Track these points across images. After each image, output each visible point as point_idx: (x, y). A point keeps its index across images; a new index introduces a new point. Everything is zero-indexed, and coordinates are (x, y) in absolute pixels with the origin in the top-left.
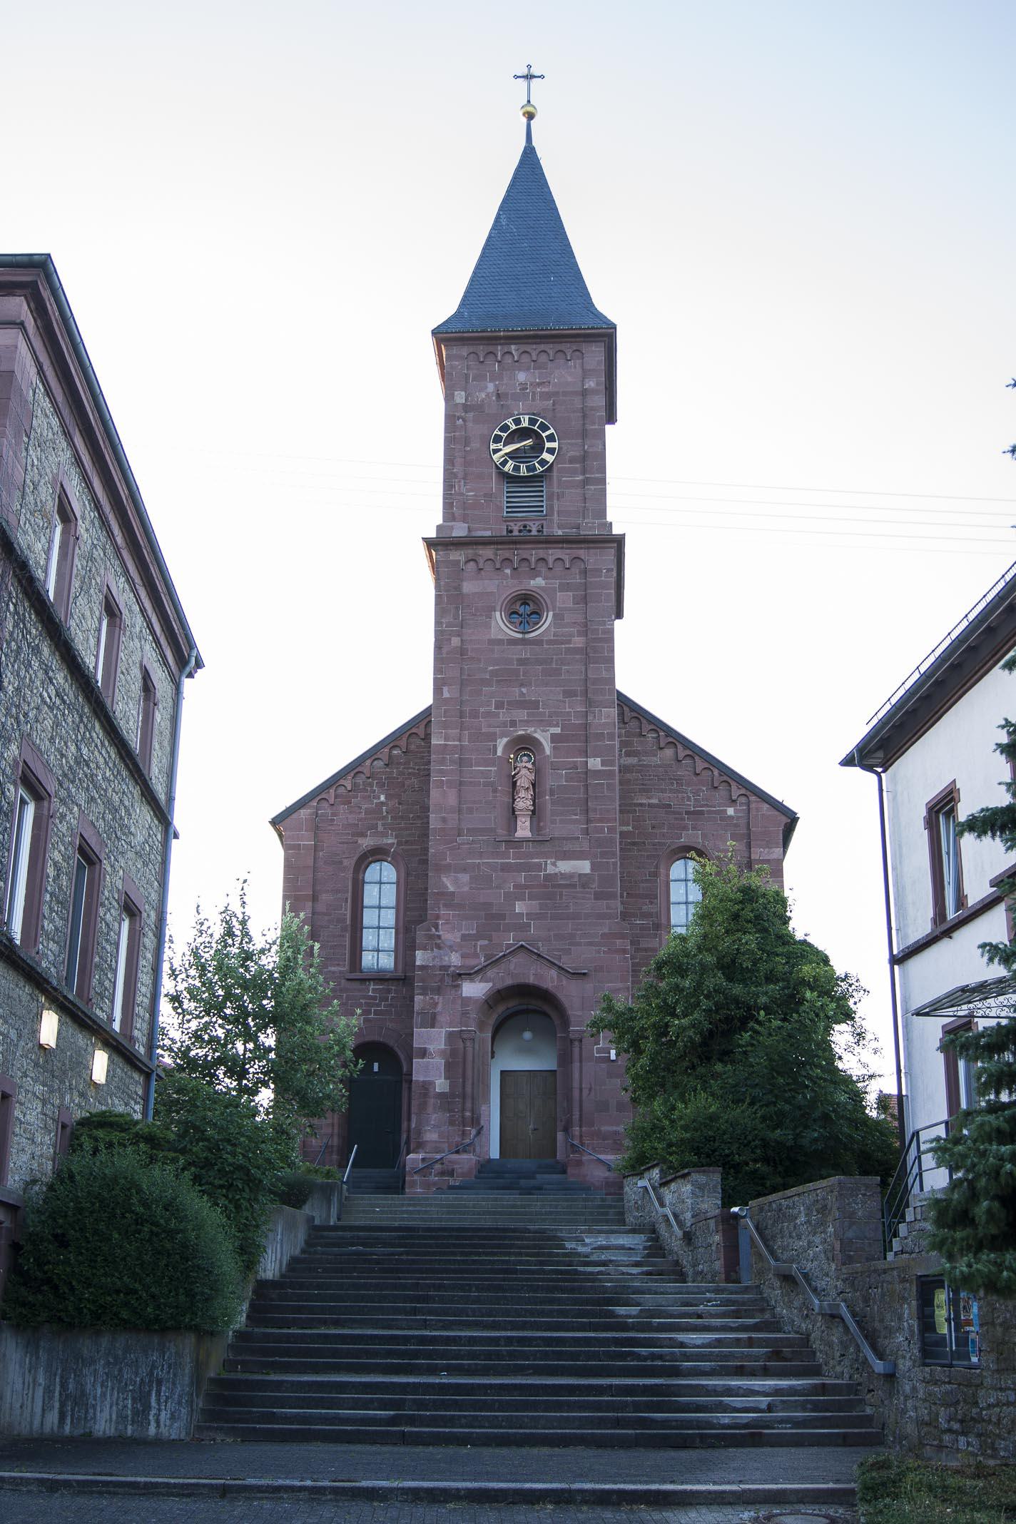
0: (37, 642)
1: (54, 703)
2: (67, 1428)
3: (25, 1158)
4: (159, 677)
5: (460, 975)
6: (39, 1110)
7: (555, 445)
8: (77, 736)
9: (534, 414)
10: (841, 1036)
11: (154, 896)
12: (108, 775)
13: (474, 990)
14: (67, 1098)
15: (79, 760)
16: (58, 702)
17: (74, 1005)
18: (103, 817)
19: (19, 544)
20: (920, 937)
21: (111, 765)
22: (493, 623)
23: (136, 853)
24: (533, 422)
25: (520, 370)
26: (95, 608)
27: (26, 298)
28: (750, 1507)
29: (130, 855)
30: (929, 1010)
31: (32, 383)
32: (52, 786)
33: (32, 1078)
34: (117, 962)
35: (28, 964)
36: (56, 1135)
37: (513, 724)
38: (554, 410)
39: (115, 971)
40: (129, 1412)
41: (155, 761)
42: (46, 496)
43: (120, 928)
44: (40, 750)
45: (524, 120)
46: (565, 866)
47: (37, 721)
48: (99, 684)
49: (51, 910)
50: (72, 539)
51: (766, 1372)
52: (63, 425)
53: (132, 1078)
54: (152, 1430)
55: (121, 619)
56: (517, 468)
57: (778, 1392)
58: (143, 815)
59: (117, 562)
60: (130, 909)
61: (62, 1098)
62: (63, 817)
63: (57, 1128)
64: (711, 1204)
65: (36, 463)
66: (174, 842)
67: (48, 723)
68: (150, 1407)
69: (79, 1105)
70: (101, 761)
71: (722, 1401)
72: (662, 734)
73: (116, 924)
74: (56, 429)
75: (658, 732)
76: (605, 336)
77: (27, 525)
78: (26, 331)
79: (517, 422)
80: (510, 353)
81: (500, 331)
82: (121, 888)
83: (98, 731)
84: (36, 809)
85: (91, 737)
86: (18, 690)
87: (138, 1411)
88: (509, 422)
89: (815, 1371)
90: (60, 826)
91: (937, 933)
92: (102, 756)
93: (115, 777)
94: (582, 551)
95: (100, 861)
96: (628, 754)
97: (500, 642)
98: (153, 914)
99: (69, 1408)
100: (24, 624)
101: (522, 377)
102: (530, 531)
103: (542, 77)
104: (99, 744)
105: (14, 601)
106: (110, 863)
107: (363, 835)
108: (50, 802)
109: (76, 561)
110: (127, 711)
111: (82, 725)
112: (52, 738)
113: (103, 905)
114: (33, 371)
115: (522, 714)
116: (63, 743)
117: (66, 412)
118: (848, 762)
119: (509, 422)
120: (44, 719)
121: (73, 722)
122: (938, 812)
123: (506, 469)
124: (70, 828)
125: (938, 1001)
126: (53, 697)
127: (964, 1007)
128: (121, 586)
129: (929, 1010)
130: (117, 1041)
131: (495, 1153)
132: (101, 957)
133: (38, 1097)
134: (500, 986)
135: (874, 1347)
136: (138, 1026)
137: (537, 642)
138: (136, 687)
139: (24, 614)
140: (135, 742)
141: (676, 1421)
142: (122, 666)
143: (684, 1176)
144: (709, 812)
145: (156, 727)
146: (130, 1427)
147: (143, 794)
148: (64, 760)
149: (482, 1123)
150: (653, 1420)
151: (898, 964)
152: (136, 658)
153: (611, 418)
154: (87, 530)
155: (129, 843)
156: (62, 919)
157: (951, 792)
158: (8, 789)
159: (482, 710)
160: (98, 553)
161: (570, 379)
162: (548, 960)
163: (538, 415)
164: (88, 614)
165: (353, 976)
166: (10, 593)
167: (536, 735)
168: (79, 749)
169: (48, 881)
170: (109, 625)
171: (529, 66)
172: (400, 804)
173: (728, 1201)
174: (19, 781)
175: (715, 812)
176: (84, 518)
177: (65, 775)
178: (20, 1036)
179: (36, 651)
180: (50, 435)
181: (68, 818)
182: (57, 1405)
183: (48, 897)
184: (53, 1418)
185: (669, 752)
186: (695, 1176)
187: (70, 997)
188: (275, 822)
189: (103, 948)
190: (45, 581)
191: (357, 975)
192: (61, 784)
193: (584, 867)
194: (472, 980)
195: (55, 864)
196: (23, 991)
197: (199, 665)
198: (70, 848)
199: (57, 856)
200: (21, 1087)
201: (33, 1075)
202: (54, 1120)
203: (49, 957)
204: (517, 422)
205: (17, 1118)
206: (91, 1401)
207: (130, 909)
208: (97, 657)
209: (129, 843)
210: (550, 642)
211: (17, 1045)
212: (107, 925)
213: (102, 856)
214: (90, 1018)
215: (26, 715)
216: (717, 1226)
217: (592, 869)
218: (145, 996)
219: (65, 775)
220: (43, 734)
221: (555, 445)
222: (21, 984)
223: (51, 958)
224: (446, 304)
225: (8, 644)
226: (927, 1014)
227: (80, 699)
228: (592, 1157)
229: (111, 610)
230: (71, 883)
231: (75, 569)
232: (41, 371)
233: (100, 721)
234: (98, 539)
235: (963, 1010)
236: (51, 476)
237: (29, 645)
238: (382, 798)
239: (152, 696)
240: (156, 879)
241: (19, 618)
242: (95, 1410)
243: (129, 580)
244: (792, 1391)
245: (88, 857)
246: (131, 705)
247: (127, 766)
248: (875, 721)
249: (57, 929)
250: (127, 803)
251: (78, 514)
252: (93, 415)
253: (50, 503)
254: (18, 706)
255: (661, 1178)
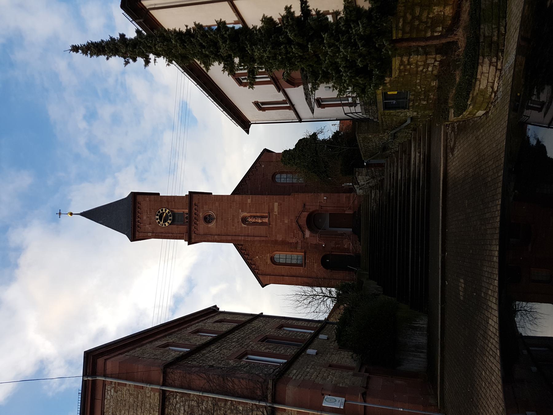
0: (201, 355)
1: (220, 349)
2: (425, 351)
3: (348, 360)
4: (217, 318)
5: (303, 238)
6: (334, 356)
7: (164, 209)
8: (230, 342)
9: (155, 215)
10: (320, 137)
11: (278, 320)
12: (242, 333)
13: (308, 233)
14: (331, 347)
15: (237, 342)
16: (220, 348)
17: (305, 344)
18: (254, 335)
19: (171, 360)
20: (294, 113)
21: (240, 332)
22: (212, 227)
23: (265, 325)
24: (157, 215)
25: (143, 218)
26: (195, 337)
27: (98, 358)
28: (448, 155)
29: (266, 327)
30: (313, 111)
31: (124, 356)
32: (243, 350)
33: (325, 358)
34: (295, 331)
35: (293, 358)
36: (342, 351)
37: (238, 222)
38: (154, 209)
39: (297, 332)
40: (420, 332)
41: (241, 319)
42: (158, 352)
43: (286, 330)
44: (233, 353)
45: (73, 215)
46: (276, 209)
47: (224, 354)
48: (216, 335)
49: (279, 350)
50: (173, 344)
51: (410, 155)
52: (139, 347)
53: (327, 327)
54: (425, 326)
55: (199, 329)
56: (170, 220)
57: (415, 150)
58: (255, 323)
59: (183, 330)
60: (281, 327)
61: (331, 348)
62: (252, 347)
63: (340, 350)
64: (364, 171)
65: (148, 355)
66: (264, 314)
67: (225, 351)
68: (419, 326)
69: (334, 344)
70: (238, 335)
71: (417, 166)
72: (242, 183)
73: (285, 331)
74: (140, 349)
75: (242, 185)
76: (134, 196)
77: (166, 357)
78: (107, 359)
79: (157, 219)
80: (138, 221)
81: (132, 223)
82: (274, 330)
83: (230, 336)
84: (249, 355)
85: (231, 338)
86: (214, 360)
87: (420, 330)
88: (157, 221)
89: (410, 142)
90: (255, 348)
91: (293, 108)
92: (237, 335)
93: (243, 331)
94: (193, 203)
95: (266, 336)
96: (248, 192)
97: (216, 225)
98: (283, 320)
99: (420, 350)
100: (195, 358)
101: (145, 218)
102: (187, 216)
103: (60, 210)
104: (233, 336)
105: (188, 362)
106: (267, 333)
107: (267, 262)
108: (248, 351)
109: (180, 342)
110: (225, 327)
111: (227, 341)
112: (229, 350)
113: (279, 335)
114: (120, 356)
115: (236, 220)
116: (232, 347)
117: (135, 346)
118: (248, 132)
119: (157, 221)
120: (224, 352)
121: (226, 343)
122: (241, 82)
123: (170, 222)
124: (256, 344)
125: (310, 109)
126: (218, 349)
127: (312, 100)
128: (190, 329)
129: (313, 111)
130: (317, 331)
131: (351, 230)
132: (293, 336)
133: (331, 356)
134: (307, 228)
135: (402, 124)
136: (313, 325)
137: (217, 215)
138: (219, 324)
139: (193, 358)
140: (235, 325)
141: (422, 178)
142: (213, 329)
143: (356, 178)
144: (263, 171)
145: (231, 319)
146: (425, 333)
147: (249, 323)
148: (237, 346)
149: (342, 233)
150: (423, 184)
151: (302, 120)
152: (211, 324)
153: (158, 194)
154: (172, 339)
155: (263, 327)
156: (281, 347)
157: (255, 103)
158: (242, 363)
159: (234, 230)
160: (179, 336)
161: (146, 205)
162: (300, 214)
163: (156, 214)
164: (196, 339)
165: (304, 266)
166: (185, 363)
167: (241, 216)
168: (234, 342)
169: (270, 351)
170: (201, 333)
171: (57, 214)
172: (259, 253)
173: (363, 166)
174: (240, 360)
175: (263, 170)
176: (168, 340)
177: (241, 346)
178: (313, 361)
179: (204, 355)
180: (141, 350)
181: (253, 345)
182: (419, 354)
183: (274, 352)
184: (422, 355)
185: (247, 182)
186: (357, 176)
187: (303, 345)
188: (263, 286)
189: (290, 335)
190: (184, 352)
191: (304, 264)
192: (243, 347)
193: (276, 204)
194: (305, 234)
195: (265, 349)
196: (301, 360)
197: (215, 306)
198: (262, 345)
199: (263, 349)
200: (328, 361)
201: (324, 357)
202: (337, 351)
203: (291, 351)
204: (157, 219)
205: (336, 362)
206: (417, 343)
207: (281, 327)
208: (209, 336)
209: (263, 327)
210: (217, 212)
211: (316, 362)
212: (284, 334)
213: (265, 335)
214: (310, 339)
215: (222, 358)
216: (369, 169)
217: (277, 202)
218: (305, 323)
219: (241, 346)
220: (228, 353)
221: (164, 209)
222: (298, 360)
223: (292, 351)
224: (124, 238)
225: (200, 363)
226: (313, 110)
227: (220, 341)
228: (352, 204)
229: (196, 332)
230: (271, 344)
231: (183, 343)
232: (121, 354)
233: (227, 335)
234: (175, 336)
235: (313, 100)
236: (153, 350)
237: (201, 357)
238: (257, 257)
239: (222, 320)
240: (273, 319)
241: (193, 360)
242: (420, 342)
243: (188, 327)
244: (415, 147)
245: (265, 339)
246: (224, 326)
247: (240, 328)
248: (237, 124)
249: (284, 349)
250: (251, 328)
251: (167, 342)
252: (137, 338)
253: (161, 351)
254: (219, 360)
255: (357, 185)
